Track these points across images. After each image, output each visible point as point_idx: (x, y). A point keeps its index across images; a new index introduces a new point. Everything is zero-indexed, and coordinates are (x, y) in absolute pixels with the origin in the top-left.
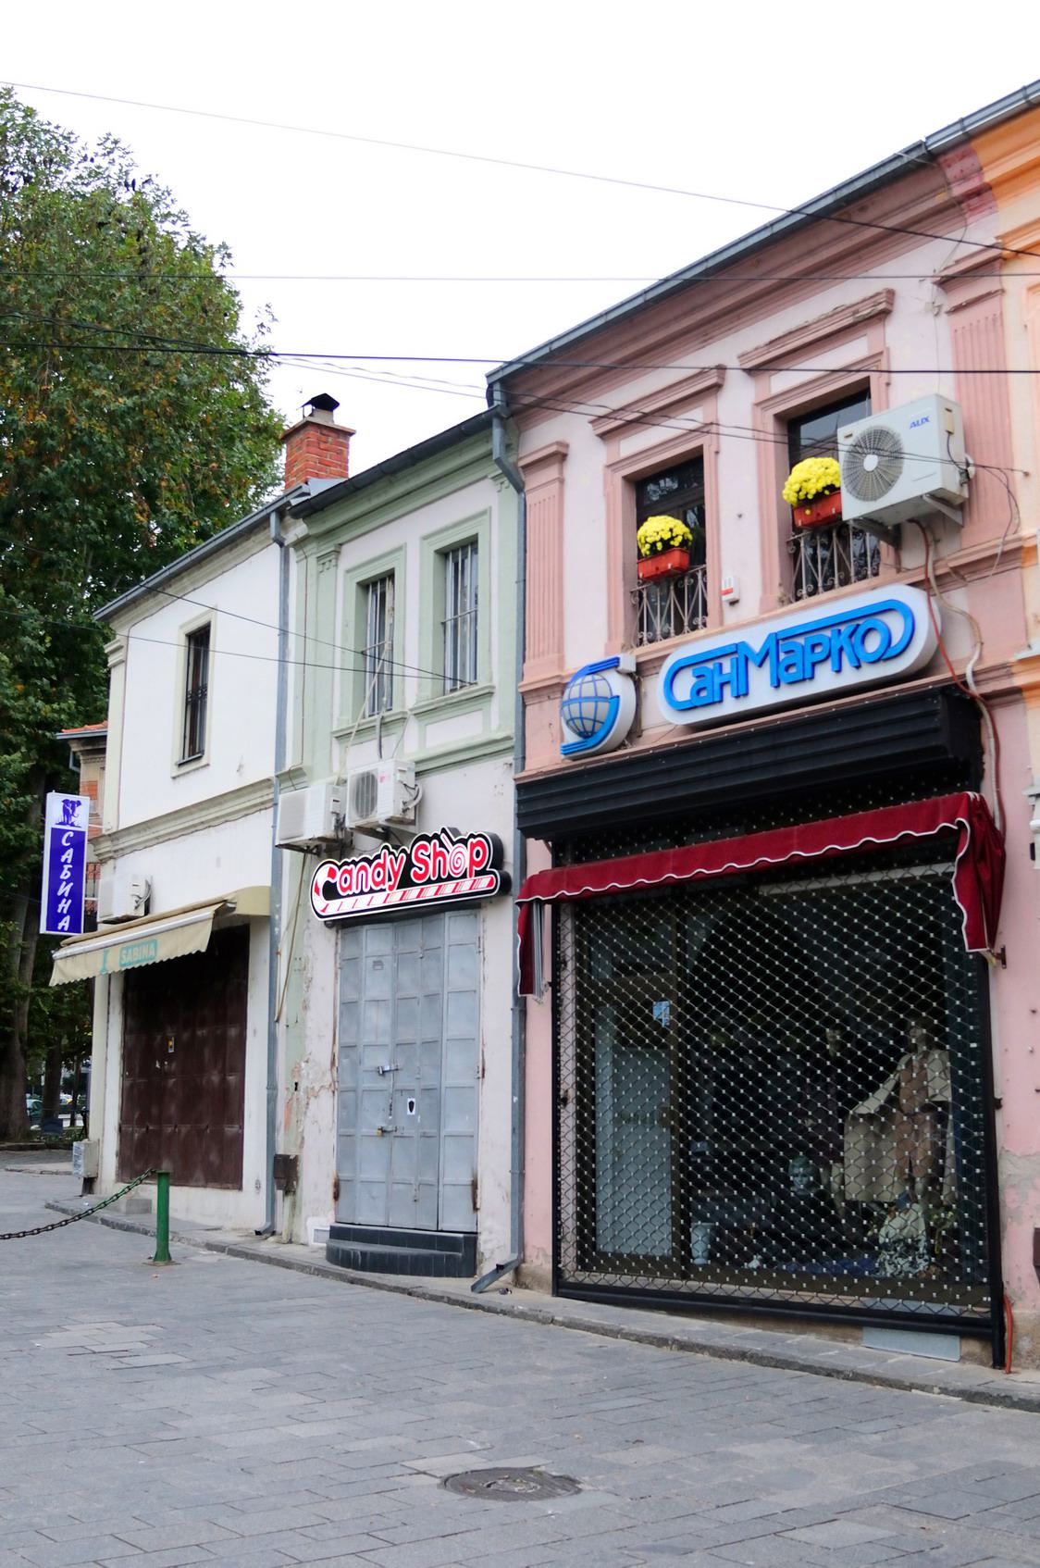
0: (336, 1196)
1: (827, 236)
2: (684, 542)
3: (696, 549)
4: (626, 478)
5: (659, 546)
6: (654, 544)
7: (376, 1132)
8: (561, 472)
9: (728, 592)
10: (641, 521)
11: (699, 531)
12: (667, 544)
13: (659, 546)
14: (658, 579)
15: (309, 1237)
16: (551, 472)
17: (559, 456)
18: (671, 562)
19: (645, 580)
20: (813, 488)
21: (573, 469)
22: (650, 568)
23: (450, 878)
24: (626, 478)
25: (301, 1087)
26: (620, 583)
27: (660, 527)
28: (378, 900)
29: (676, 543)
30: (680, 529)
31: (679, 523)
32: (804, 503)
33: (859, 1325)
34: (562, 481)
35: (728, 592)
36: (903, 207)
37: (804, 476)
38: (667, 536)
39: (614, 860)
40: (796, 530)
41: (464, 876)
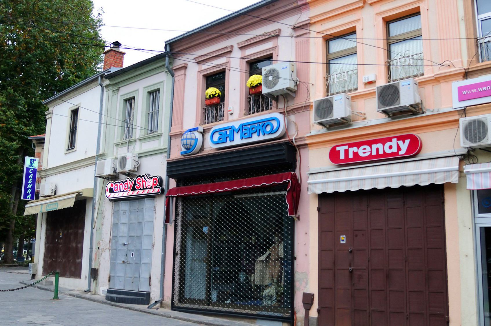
0: (109, 281)
1: (233, 24)
2: (219, 95)
3: (222, 98)
4: (204, 75)
5: (212, 96)
6: (210, 96)
7: (122, 262)
8: (185, 72)
9: (230, 111)
10: (207, 88)
11: (223, 90)
12: (214, 96)
13: (212, 96)
14: (211, 105)
15: (101, 293)
16: (182, 72)
17: (185, 67)
18: (214, 101)
19: (207, 105)
20: (255, 83)
21: (189, 71)
22: (209, 102)
23: (147, 188)
24: (204, 75)
25: (100, 248)
26: (200, 106)
27: (212, 90)
28: (125, 194)
29: (216, 95)
30: (218, 91)
31: (217, 90)
32: (252, 87)
33: (256, 319)
34: (185, 75)
35: (230, 111)
36: (285, 6)
37: (253, 80)
38: (214, 93)
39: (194, 186)
40: (250, 95)
41: (151, 188)
